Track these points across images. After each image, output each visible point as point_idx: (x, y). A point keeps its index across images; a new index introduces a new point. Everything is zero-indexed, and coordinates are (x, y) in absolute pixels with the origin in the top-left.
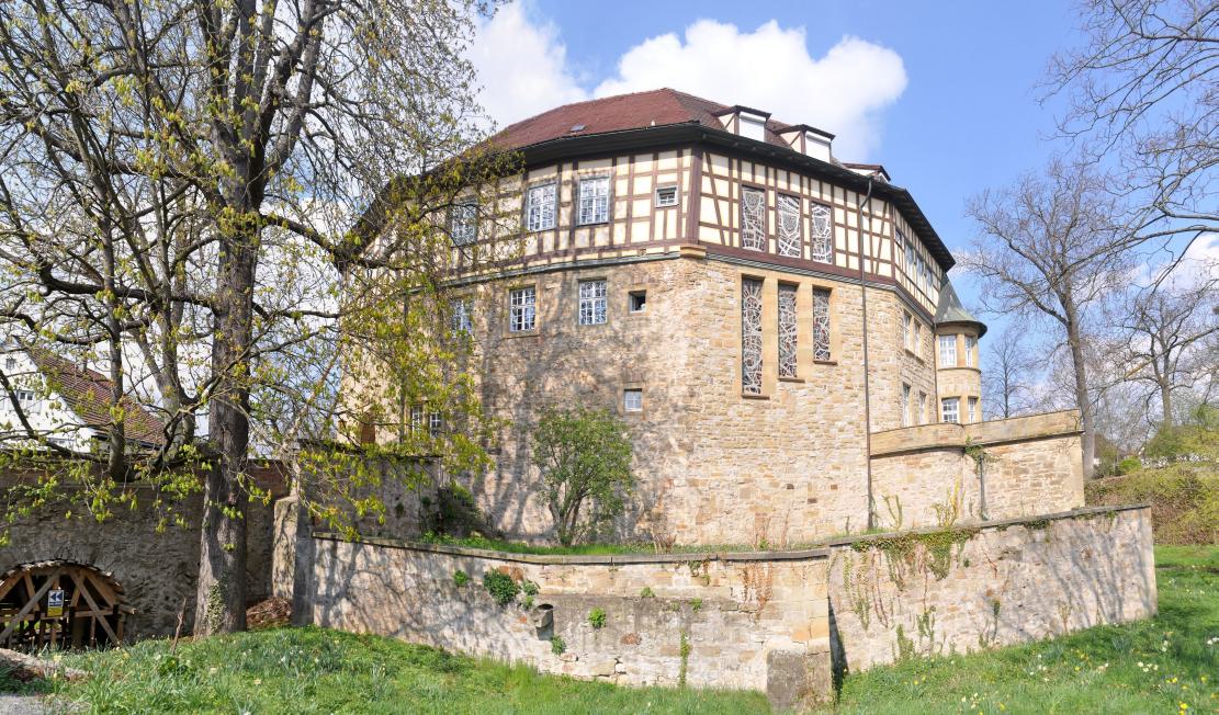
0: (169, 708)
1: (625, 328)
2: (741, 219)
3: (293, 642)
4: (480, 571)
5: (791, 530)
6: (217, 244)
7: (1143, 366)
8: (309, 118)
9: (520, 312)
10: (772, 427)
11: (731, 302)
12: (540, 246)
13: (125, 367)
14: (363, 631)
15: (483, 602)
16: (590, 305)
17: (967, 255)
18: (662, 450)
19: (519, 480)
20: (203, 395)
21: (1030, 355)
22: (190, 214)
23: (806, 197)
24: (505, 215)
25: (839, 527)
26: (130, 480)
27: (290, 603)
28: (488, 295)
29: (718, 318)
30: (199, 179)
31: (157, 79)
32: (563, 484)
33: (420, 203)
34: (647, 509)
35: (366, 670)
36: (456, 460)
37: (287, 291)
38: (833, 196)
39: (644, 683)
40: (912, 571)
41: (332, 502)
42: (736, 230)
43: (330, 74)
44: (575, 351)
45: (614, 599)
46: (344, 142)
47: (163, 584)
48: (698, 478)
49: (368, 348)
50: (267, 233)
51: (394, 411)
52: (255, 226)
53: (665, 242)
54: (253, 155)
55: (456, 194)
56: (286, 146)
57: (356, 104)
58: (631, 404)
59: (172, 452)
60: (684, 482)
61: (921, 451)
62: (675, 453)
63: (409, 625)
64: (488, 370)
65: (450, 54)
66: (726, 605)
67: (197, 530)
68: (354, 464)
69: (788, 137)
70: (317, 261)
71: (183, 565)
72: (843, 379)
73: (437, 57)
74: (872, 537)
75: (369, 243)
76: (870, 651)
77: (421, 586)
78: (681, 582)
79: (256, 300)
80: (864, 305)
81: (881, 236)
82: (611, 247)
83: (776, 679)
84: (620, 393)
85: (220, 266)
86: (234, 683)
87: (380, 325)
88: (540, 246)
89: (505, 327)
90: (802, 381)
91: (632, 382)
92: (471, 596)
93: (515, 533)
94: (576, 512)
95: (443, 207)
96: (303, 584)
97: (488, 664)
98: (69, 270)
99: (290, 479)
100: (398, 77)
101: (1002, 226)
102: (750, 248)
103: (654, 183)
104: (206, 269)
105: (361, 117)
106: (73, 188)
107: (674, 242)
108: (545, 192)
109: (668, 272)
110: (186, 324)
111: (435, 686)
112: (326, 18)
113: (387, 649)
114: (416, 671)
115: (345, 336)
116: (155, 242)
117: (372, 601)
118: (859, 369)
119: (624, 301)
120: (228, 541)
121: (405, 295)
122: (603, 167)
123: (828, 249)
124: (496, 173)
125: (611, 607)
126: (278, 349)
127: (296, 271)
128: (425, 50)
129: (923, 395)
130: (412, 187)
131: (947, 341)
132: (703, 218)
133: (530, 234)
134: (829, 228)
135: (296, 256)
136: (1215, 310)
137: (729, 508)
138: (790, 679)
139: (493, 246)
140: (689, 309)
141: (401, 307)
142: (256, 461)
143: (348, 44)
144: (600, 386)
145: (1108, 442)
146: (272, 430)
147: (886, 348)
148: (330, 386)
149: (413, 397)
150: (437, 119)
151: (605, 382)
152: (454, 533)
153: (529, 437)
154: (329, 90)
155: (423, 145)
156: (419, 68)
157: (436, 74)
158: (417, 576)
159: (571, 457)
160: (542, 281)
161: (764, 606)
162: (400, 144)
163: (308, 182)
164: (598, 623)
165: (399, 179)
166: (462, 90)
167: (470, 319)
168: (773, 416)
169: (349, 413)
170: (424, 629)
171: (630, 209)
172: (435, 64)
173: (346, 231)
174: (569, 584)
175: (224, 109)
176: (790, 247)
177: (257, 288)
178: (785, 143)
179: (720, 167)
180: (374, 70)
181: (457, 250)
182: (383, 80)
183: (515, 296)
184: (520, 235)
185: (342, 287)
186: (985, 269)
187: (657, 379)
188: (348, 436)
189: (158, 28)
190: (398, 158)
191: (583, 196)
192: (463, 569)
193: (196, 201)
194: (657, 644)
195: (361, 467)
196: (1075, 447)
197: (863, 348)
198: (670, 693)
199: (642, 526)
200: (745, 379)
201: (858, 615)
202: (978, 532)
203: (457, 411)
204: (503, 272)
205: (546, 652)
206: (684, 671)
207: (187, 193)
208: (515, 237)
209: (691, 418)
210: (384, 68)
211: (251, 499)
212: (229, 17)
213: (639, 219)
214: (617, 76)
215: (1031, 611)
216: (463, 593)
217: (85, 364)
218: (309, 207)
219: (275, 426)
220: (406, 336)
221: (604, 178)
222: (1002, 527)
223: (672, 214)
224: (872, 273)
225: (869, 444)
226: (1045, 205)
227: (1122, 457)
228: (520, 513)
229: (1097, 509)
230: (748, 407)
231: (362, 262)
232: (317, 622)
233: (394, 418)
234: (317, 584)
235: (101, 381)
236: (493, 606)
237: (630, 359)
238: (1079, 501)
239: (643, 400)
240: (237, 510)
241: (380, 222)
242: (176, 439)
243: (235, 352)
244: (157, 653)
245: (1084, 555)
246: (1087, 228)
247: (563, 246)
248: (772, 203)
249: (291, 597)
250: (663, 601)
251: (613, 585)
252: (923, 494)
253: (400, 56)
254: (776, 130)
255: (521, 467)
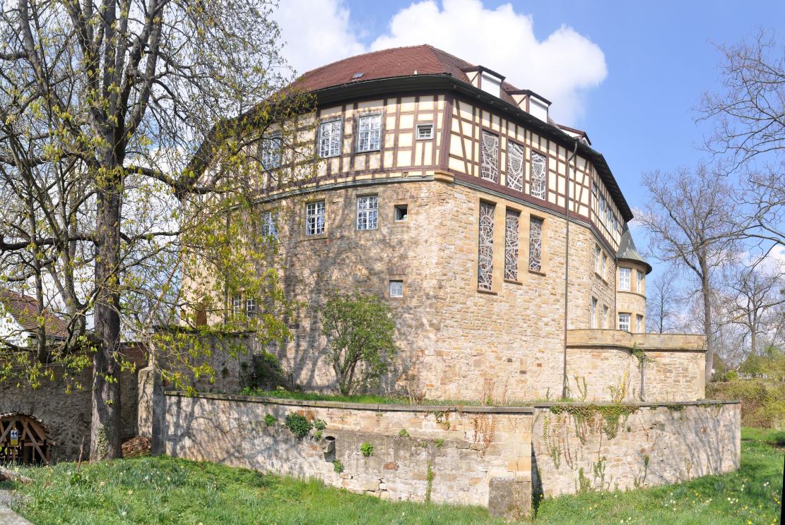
0: (77, 505)
1: (391, 233)
2: (481, 155)
3: (153, 466)
4: (283, 415)
5: (509, 392)
6: (95, 195)
7: (743, 315)
8: (156, 87)
9: (313, 220)
10: (498, 316)
11: (471, 218)
12: (329, 169)
13: (44, 290)
14: (200, 459)
15: (285, 437)
16: (365, 214)
17: (642, 214)
18: (417, 328)
19: (312, 347)
20: (90, 301)
21: (678, 294)
22: (78, 179)
23: (528, 146)
24: (303, 144)
25: (541, 394)
26: (50, 362)
27: (150, 440)
28: (289, 207)
29: (461, 229)
30: (83, 153)
31: (55, 93)
32: (344, 350)
33: (238, 139)
34: (405, 371)
35: (203, 486)
36: (266, 333)
37: (142, 220)
38: (548, 148)
39: (400, 498)
40: (592, 432)
41: (177, 369)
42: (476, 164)
43: (169, 49)
44: (353, 250)
45: (380, 437)
46: (180, 100)
47: (71, 427)
48: (443, 350)
49: (200, 255)
50: (128, 180)
51: (220, 300)
52: (120, 176)
53: (423, 168)
54: (117, 126)
55: (265, 130)
56: (139, 113)
57: (189, 68)
58: (395, 292)
59: (73, 342)
60: (432, 353)
61: (603, 347)
62: (427, 331)
63: (233, 455)
64: (289, 265)
65: (260, 17)
66: (462, 444)
67: (89, 392)
68: (192, 341)
69: (517, 98)
70: (163, 194)
71: (82, 415)
72: (550, 287)
73: (249, 20)
74: (564, 404)
75: (200, 174)
76: (559, 484)
77: (241, 427)
78: (429, 426)
79: (123, 230)
80: (567, 235)
81: (582, 185)
82: (382, 170)
83: (495, 497)
84: (386, 283)
85: (98, 211)
86: (115, 492)
87: (209, 237)
88: (329, 169)
89: (302, 232)
90: (521, 284)
91: (396, 275)
92: (277, 432)
93: (309, 385)
94: (353, 370)
95: (255, 141)
96: (158, 428)
97: (289, 481)
98: (12, 236)
99: (148, 355)
100: (220, 40)
101: (666, 199)
102: (486, 179)
103: (416, 121)
104: (89, 215)
105: (193, 77)
106: (12, 184)
107: (429, 168)
108: (333, 127)
109: (424, 191)
110: (78, 255)
111: (251, 497)
112: (165, 7)
113: (217, 471)
114: (238, 486)
115: (184, 248)
116: (58, 204)
117: (206, 438)
118: (561, 281)
119: (391, 212)
120: (109, 399)
121: (227, 212)
122: (377, 107)
123: (542, 189)
124: (295, 112)
125: (377, 442)
126: (138, 263)
127: (148, 204)
128: (241, 15)
129: (606, 308)
130: (231, 127)
131: (625, 272)
132: (452, 152)
133: (321, 160)
134: (545, 173)
135: (148, 193)
136: (782, 292)
137: (465, 374)
138: (503, 496)
139: (293, 169)
140: (440, 221)
141: (225, 222)
142: (126, 344)
143: (182, 21)
144: (372, 277)
145: (721, 360)
146: (135, 321)
147: (582, 269)
148: (174, 286)
149: (234, 288)
150: (250, 70)
151: (375, 274)
152: (265, 387)
153: (320, 315)
154: (169, 61)
155: (240, 92)
156: (236, 30)
157: (249, 34)
158: (238, 419)
159: (350, 330)
160: (330, 196)
161: (489, 445)
162: (222, 94)
163: (155, 136)
164: (368, 453)
165: (222, 123)
166: (270, 46)
167: (276, 227)
168: (500, 307)
169: (188, 304)
170: (244, 457)
171: (396, 140)
172: (249, 26)
173: (183, 168)
174: (346, 423)
175: (96, 99)
176: (515, 182)
177: (123, 222)
178: (515, 102)
179: (466, 112)
180: (202, 37)
181: (266, 174)
182: (209, 45)
183: (309, 208)
184: (313, 161)
185: (181, 211)
186: (653, 227)
187: (414, 274)
188: (187, 321)
189: (54, 57)
190: (221, 105)
191: (361, 129)
192: (271, 413)
193: (82, 168)
194: (410, 471)
195: (197, 343)
196: (701, 359)
197: (565, 266)
198: (419, 507)
199: (401, 384)
200: (480, 278)
201: (552, 458)
202: (637, 408)
203: (267, 298)
204: (300, 190)
205: (330, 471)
206: (429, 491)
207: (75, 165)
208: (310, 162)
209: (439, 305)
210: (209, 35)
211: (122, 369)
212: (98, 29)
213: (404, 149)
214: (388, 33)
215: (669, 464)
216: (271, 430)
217: (23, 291)
218: (156, 155)
219: (137, 318)
220: (228, 243)
221: (377, 115)
222: (653, 407)
223: (429, 146)
224: (574, 212)
225: (566, 338)
226: (694, 194)
227: (727, 370)
228: (313, 371)
229: (712, 401)
230: (481, 300)
231: (195, 191)
232: (168, 452)
233: (220, 305)
234: (168, 427)
235: (31, 301)
236: (293, 440)
237: (395, 257)
238: (701, 395)
239: (404, 289)
240: (114, 377)
241: (208, 158)
242: (75, 333)
243: (109, 269)
244: (68, 470)
245: (702, 430)
246: (718, 218)
247: (345, 169)
248: (504, 147)
249: (150, 436)
250: (415, 440)
251: (378, 425)
252: (603, 378)
253: (221, 23)
254: (509, 91)
255: (314, 337)
